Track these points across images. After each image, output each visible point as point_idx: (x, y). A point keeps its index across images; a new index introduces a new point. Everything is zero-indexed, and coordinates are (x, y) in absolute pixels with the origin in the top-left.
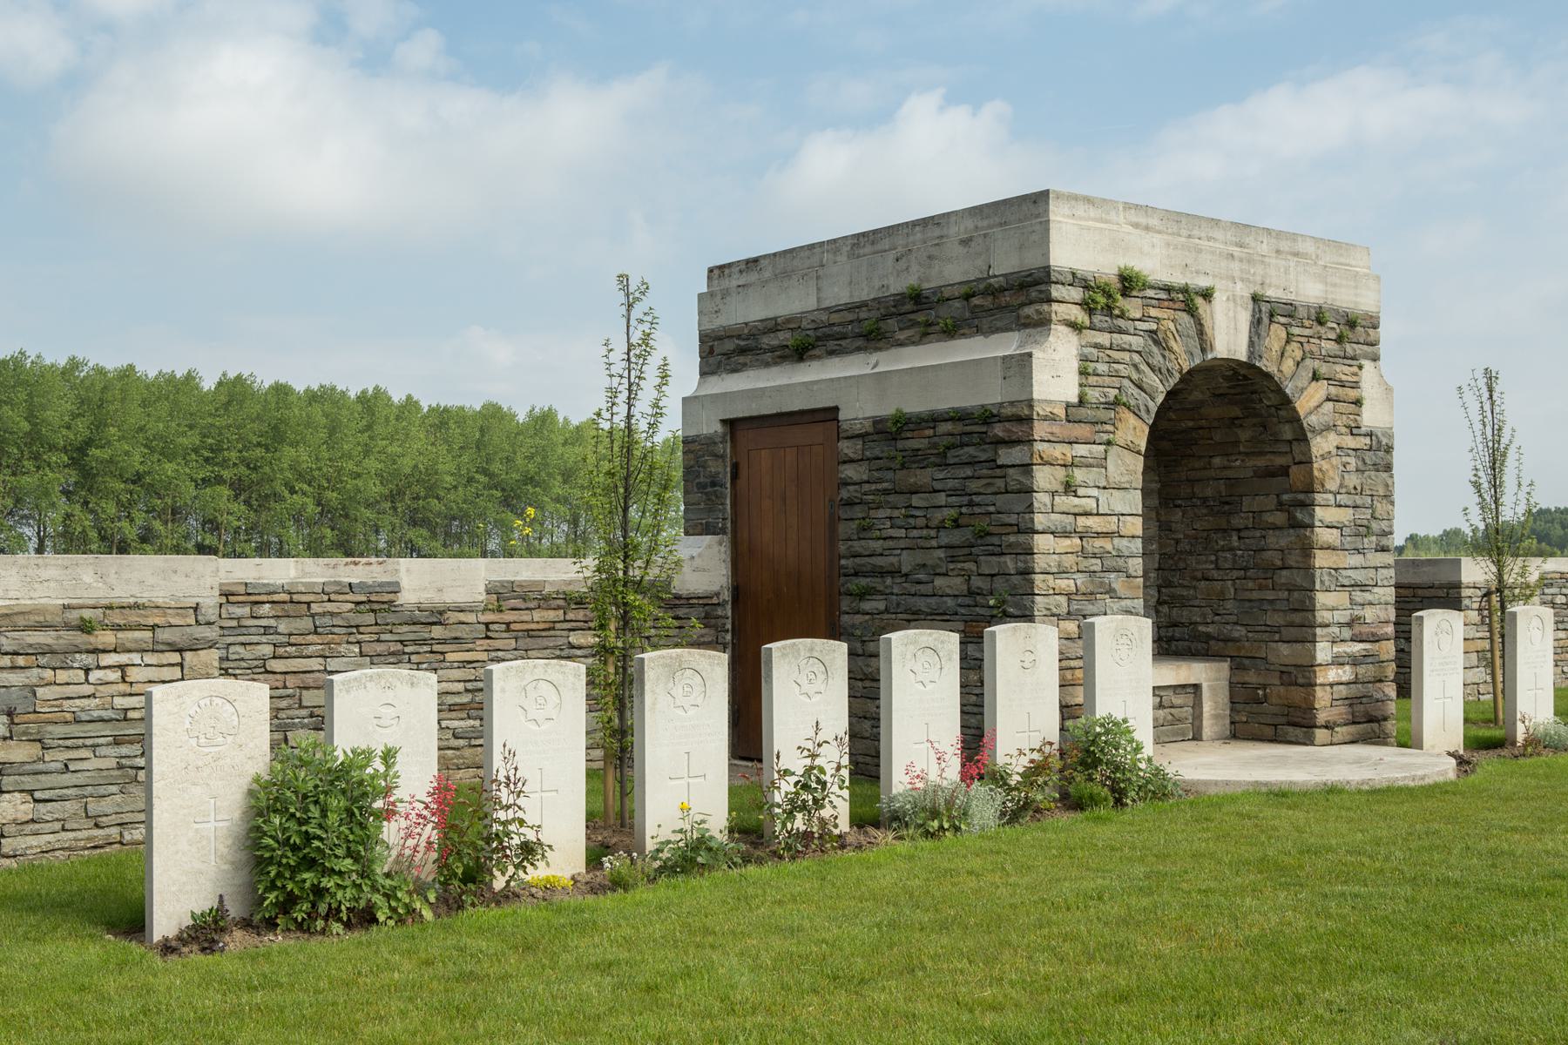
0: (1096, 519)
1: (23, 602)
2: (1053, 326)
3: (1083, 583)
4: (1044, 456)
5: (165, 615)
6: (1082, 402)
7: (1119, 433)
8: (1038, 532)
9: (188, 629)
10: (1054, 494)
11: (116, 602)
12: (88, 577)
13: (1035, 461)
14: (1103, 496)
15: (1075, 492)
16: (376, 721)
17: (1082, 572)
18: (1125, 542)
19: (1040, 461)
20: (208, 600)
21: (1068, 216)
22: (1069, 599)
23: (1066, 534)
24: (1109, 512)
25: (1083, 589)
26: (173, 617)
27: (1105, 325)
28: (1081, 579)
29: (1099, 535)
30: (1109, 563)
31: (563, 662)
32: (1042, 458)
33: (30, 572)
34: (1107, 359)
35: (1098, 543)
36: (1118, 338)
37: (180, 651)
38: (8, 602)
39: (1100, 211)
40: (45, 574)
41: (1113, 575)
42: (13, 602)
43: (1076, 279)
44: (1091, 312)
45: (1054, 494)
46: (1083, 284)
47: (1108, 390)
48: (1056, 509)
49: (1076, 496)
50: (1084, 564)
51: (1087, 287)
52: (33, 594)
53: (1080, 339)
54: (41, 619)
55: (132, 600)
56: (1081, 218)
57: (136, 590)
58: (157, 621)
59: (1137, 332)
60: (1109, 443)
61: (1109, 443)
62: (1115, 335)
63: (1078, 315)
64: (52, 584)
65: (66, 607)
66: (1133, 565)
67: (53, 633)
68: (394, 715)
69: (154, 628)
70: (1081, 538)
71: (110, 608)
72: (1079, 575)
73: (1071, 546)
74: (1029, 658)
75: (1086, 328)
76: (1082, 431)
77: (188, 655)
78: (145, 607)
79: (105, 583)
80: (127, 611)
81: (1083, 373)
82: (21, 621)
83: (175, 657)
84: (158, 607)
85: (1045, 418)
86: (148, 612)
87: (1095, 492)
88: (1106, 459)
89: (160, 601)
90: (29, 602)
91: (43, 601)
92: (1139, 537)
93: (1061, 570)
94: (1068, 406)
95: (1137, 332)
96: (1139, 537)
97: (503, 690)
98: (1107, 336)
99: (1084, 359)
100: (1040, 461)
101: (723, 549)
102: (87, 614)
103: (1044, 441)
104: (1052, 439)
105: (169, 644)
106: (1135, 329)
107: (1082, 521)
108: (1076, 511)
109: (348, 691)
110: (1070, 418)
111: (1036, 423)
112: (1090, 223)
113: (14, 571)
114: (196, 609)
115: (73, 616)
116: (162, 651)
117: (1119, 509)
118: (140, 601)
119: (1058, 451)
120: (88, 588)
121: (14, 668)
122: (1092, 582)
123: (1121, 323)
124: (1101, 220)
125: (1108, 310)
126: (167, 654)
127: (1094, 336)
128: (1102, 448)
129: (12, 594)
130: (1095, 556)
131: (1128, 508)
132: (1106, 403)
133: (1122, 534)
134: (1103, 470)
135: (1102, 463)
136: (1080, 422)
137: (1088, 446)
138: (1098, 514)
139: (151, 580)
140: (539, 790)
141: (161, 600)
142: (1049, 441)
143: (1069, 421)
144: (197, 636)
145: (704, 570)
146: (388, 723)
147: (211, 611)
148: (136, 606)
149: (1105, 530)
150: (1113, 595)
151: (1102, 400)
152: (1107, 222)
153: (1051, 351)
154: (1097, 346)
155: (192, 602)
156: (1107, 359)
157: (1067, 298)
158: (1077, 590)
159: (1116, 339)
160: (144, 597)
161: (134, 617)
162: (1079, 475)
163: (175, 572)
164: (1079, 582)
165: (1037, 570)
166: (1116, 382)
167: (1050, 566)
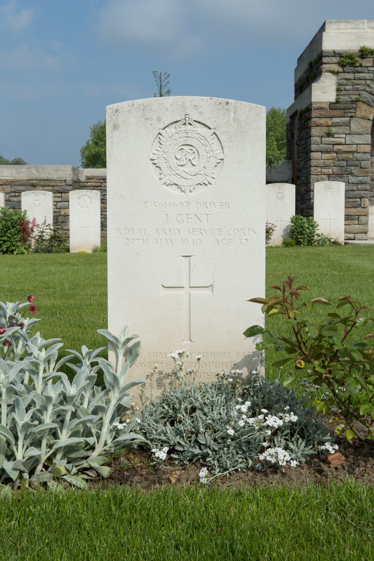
0: (345, 146)
1: (17, 178)
2: (323, 73)
3: (336, 170)
4: (316, 123)
5: (56, 183)
6: (337, 102)
7: (357, 113)
8: (313, 152)
9: (62, 187)
10: (322, 137)
11: (42, 178)
12: (34, 171)
13: (312, 125)
14: (348, 137)
15: (333, 136)
16: (34, 205)
17: (336, 166)
18: (360, 155)
19: (314, 125)
20: (69, 178)
21: (336, 29)
22: (329, 177)
23: (327, 152)
24: (351, 143)
25: (336, 173)
26: (59, 183)
27: (351, 70)
28: (335, 169)
29: (346, 152)
30: (349, 163)
31: (92, 190)
32: (315, 124)
33: (18, 170)
34: (352, 84)
35: (344, 155)
36: (358, 75)
37: (61, 193)
38: (12, 178)
39: (353, 25)
40: (23, 170)
41: (353, 168)
42: (14, 178)
43: (335, 54)
44: (343, 66)
45: (322, 137)
46: (340, 56)
47: (352, 96)
48: (323, 143)
49: (334, 137)
50: (337, 163)
51: (341, 57)
52: (20, 176)
53: (337, 77)
54: (21, 183)
55: (46, 178)
56: (342, 29)
57: (47, 175)
58: (54, 184)
59: (369, 72)
60: (351, 117)
61: (351, 117)
62: (356, 74)
63: (336, 68)
64: (24, 173)
65: (29, 180)
66: (364, 164)
67: (25, 187)
68: (39, 203)
69: (53, 186)
70: (337, 154)
71: (40, 180)
72: (335, 167)
73: (330, 157)
74: (280, 195)
75: (341, 72)
76: (339, 112)
77: (63, 194)
78: (50, 180)
79: (39, 173)
80: (45, 181)
81: (338, 90)
82: (17, 183)
83: (60, 195)
84: (54, 180)
85: (317, 109)
86: (51, 182)
87: (344, 136)
88: (350, 123)
89: (55, 178)
90: (18, 178)
91: (22, 178)
92: (368, 153)
93: (325, 165)
94: (331, 103)
95: (369, 72)
96: (368, 153)
97: (72, 198)
98: (353, 75)
99: (339, 84)
100: (314, 125)
101: (290, 165)
102: (34, 182)
103: (317, 117)
104: (321, 116)
105: (57, 191)
106: (368, 71)
107: (336, 147)
108: (333, 143)
109: (25, 196)
110: (331, 108)
111: (313, 111)
112: (348, 31)
113: (14, 169)
114: (65, 181)
115: (30, 182)
116: (56, 193)
117: (357, 142)
118: (49, 178)
119: (323, 121)
120: (34, 174)
121: (15, 196)
122: (341, 170)
123: (359, 69)
124: (354, 29)
125: (352, 65)
126: (57, 194)
127: (345, 75)
128: (348, 119)
129: (14, 176)
130: (343, 160)
131: (364, 142)
132: (352, 101)
133: (358, 151)
134: (348, 128)
135: (348, 124)
136: (336, 109)
137: (340, 118)
138: (345, 144)
139: (52, 172)
140: (185, 284)
141: (55, 178)
142: (320, 117)
143: (331, 109)
144: (65, 189)
145: (281, 173)
146: (37, 205)
147: (69, 182)
148: (48, 180)
149: (349, 150)
150: (353, 175)
151: (349, 100)
152: (357, 29)
153: (322, 83)
154: (346, 79)
155: (64, 179)
156: (352, 84)
157: (330, 62)
158: (333, 173)
159: (357, 76)
160: (50, 177)
161: (47, 183)
162: (334, 130)
163: (59, 170)
164: (334, 170)
165: (312, 165)
166: (357, 92)
167: (319, 164)
